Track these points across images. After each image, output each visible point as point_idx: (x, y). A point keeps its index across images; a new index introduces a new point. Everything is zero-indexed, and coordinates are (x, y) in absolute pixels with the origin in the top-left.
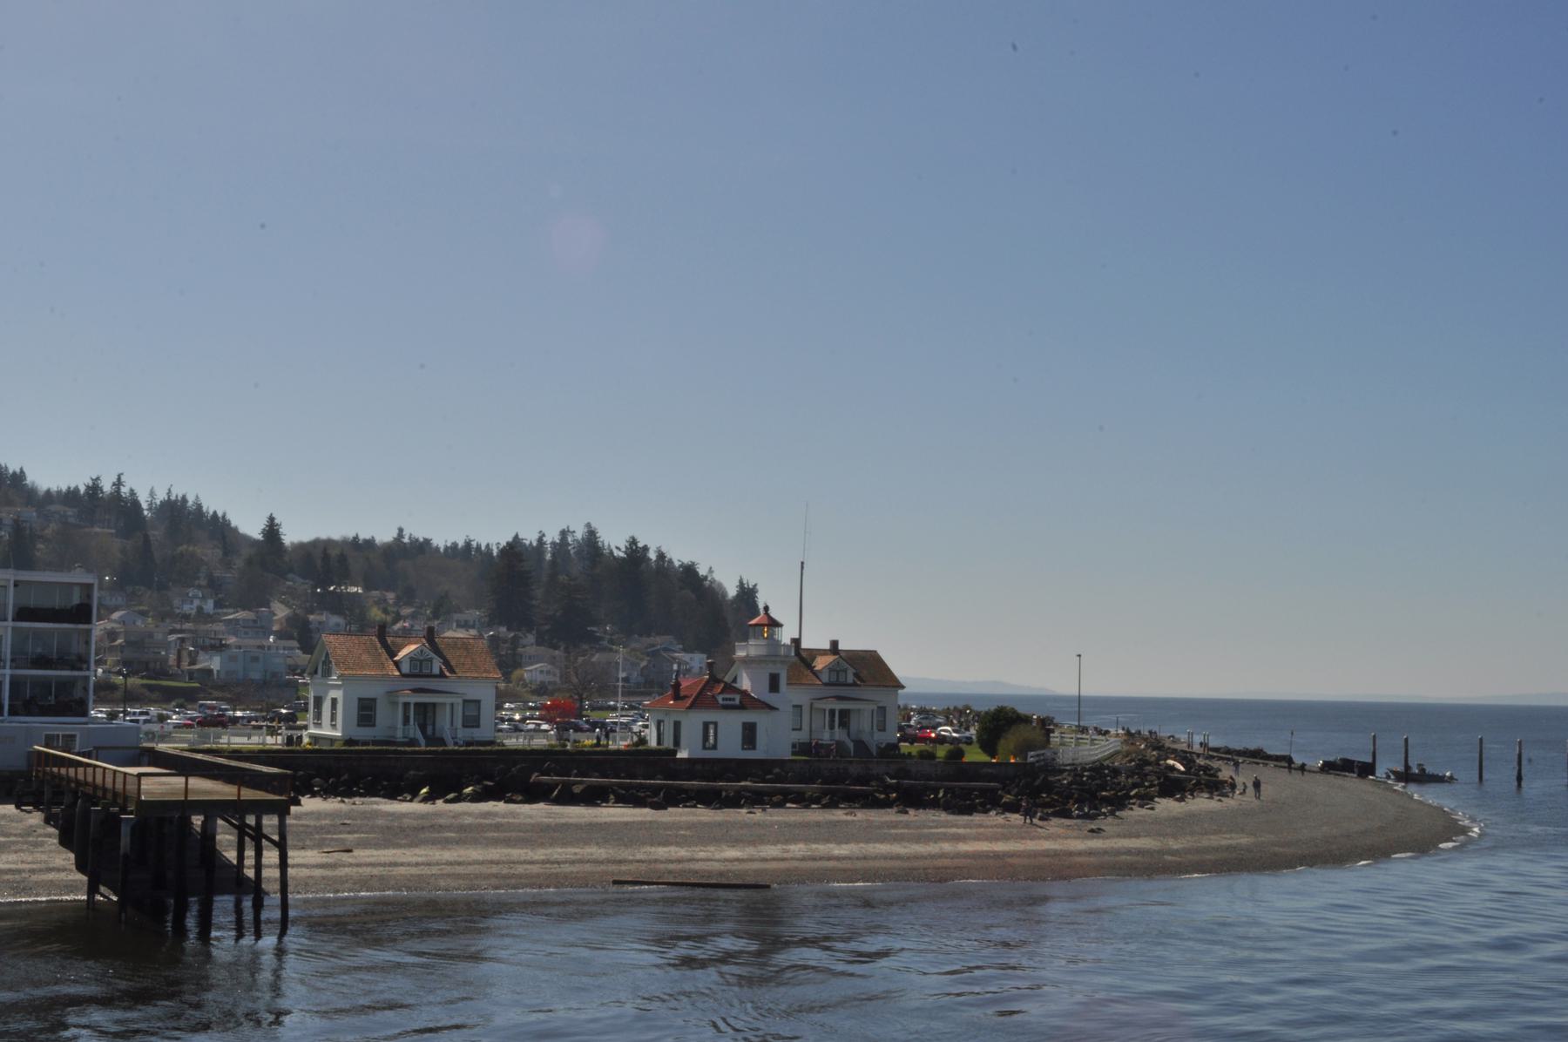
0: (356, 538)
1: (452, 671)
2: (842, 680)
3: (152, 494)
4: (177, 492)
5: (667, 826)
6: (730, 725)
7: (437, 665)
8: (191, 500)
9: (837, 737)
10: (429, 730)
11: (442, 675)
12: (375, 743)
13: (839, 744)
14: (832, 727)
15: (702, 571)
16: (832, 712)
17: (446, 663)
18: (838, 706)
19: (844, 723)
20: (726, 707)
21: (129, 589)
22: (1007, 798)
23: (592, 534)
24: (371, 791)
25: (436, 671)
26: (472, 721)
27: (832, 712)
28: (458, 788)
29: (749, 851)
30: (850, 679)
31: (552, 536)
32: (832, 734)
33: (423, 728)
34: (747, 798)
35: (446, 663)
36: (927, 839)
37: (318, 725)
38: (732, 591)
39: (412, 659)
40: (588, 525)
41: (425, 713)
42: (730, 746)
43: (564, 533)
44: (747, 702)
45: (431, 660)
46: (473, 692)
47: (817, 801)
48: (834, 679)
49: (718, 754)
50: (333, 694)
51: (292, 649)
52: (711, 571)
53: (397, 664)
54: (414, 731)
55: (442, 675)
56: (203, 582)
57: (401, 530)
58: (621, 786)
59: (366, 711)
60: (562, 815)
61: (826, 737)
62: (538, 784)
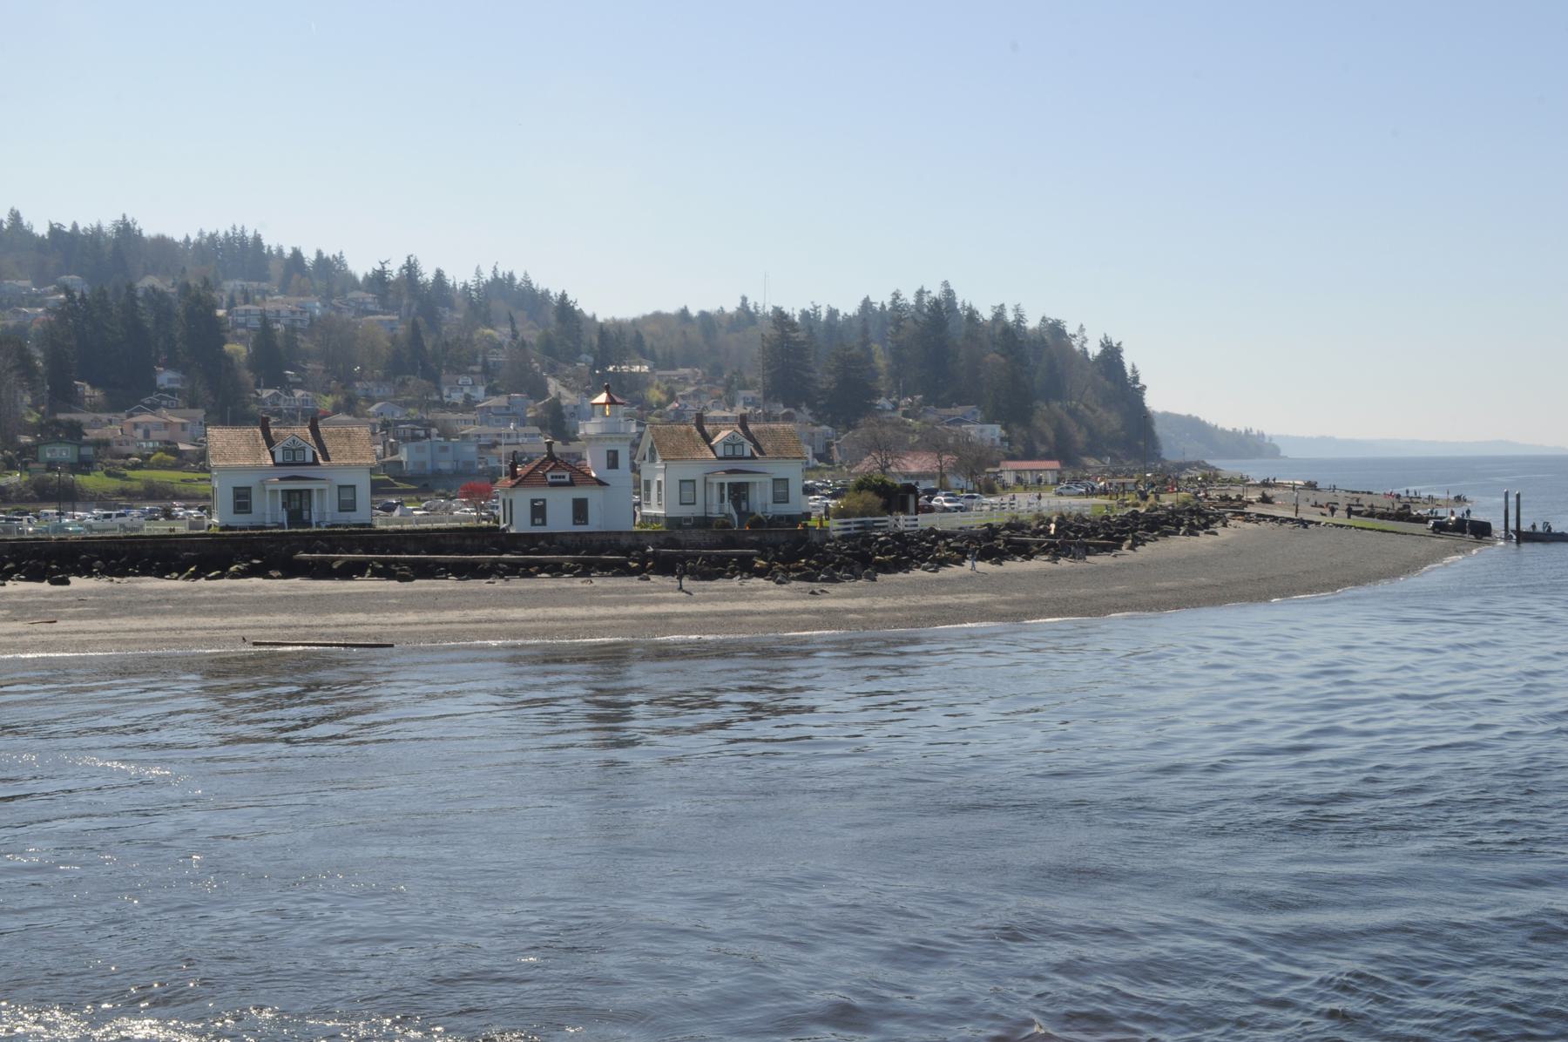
0: (684, 312)
1: (326, 457)
2: (738, 453)
3: (478, 273)
5: (412, 595)
6: (560, 505)
7: (748, 448)
8: (519, 279)
9: (726, 510)
10: (744, 505)
11: (315, 462)
12: (252, 528)
13: (728, 516)
15: (1070, 329)
16: (722, 485)
17: (757, 447)
20: (553, 485)
21: (399, 379)
22: (760, 563)
23: (564, 296)
24: (145, 572)
25: (747, 453)
29: (432, 616)
32: (721, 508)
33: (737, 506)
34: (373, 569)
35: (757, 447)
36: (657, 601)
37: (648, 505)
38: (1094, 350)
39: (726, 444)
40: (946, 284)
41: (738, 493)
42: (560, 519)
43: (920, 293)
45: (742, 444)
46: (780, 469)
47: (569, 570)
48: (729, 453)
49: (551, 528)
50: (660, 477)
51: (533, 435)
52: (1082, 329)
53: (712, 448)
54: (729, 508)
55: (753, 457)
56: (477, 369)
57: (744, 299)
58: (380, 561)
59: (242, 500)
60: (301, 588)
61: (715, 511)
62: (301, 561)
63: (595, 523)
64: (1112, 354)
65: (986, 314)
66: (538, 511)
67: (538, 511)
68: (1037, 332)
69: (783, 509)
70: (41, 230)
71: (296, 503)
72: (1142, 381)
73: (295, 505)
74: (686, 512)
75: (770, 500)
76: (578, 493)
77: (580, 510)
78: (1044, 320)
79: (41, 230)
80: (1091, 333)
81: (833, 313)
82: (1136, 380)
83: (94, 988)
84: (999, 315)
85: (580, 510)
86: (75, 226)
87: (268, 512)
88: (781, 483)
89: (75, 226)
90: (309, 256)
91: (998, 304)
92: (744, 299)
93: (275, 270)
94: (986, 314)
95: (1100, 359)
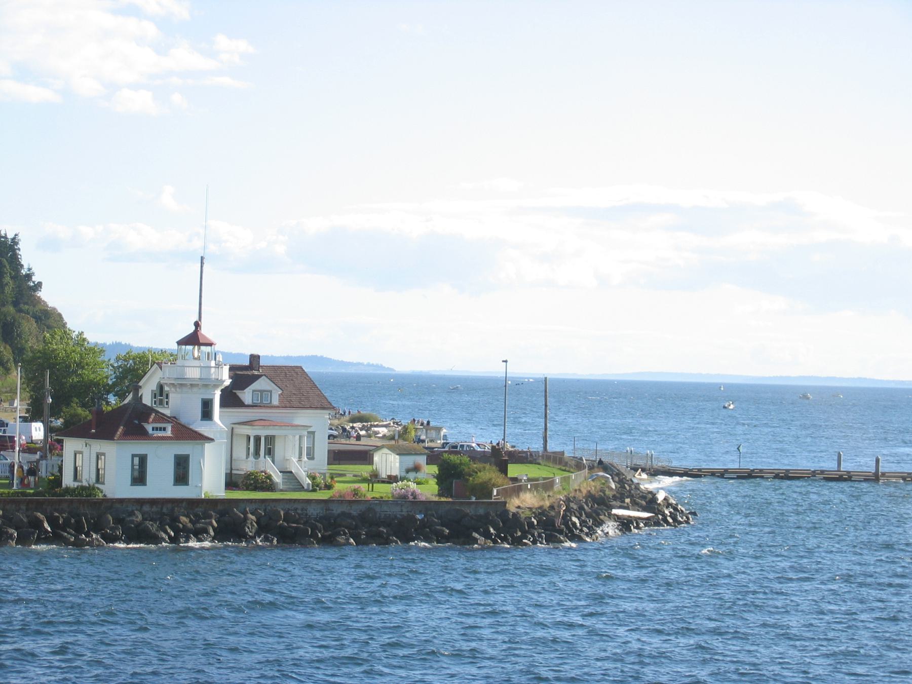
14: (257, 453)
16: (258, 439)
18: (263, 433)
19: (270, 452)
27: (258, 439)
30: (276, 401)
44: (185, 433)
76: (183, 448)
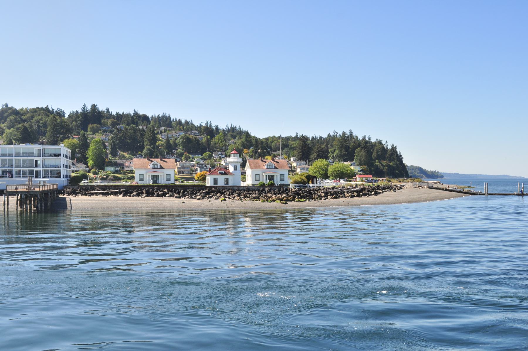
3: (227, 126)
4: (233, 125)
8: (238, 127)
26: (168, 179)
28: (132, 193)
31: (340, 133)
38: (389, 147)
40: (351, 130)
41: (271, 178)
42: (221, 182)
59: (141, 179)
63: (230, 184)
64: (394, 149)
65: (360, 138)
66: (215, 181)
67: (215, 181)
68: (375, 143)
69: (283, 182)
70: (114, 113)
71: (155, 178)
72: (402, 157)
73: (155, 179)
74: (257, 183)
75: (279, 179)
76: (226, 176)
77: (227, 180)
78: (377, 140)
79: (114, 113)
80: (389, 142)
81: (321, 137)
82: (401, 156)
83: (238, 320)
84: (364, 138)
85: (227, 180)
86: (123, 113)
87: (148, 181)
88: (282, 176)
89: (123, 113)
90: (183, 121)
91: (363, 135)
92: (297, 134)
93: (174, 124)
94: (360, 138)
95: (391, 150)
